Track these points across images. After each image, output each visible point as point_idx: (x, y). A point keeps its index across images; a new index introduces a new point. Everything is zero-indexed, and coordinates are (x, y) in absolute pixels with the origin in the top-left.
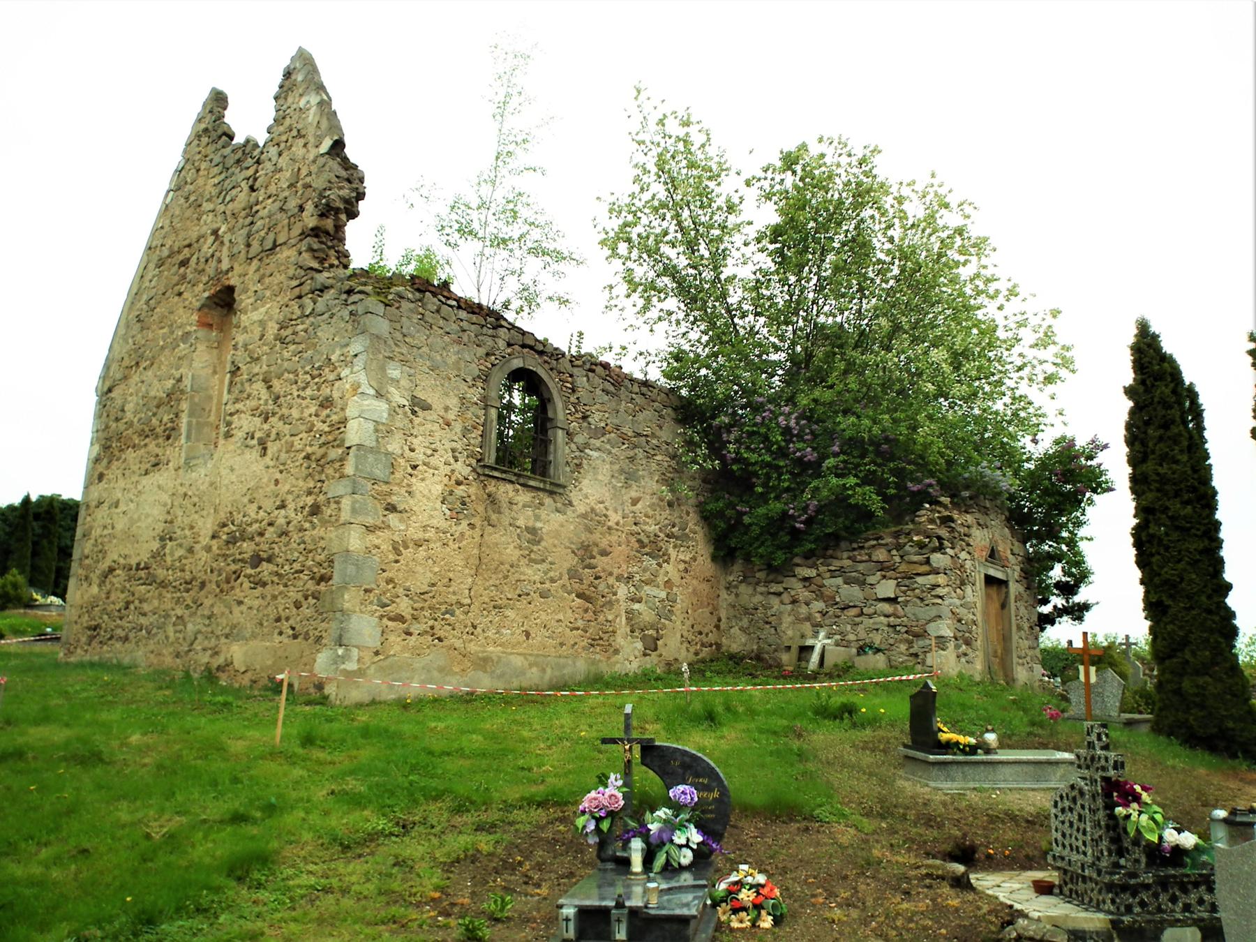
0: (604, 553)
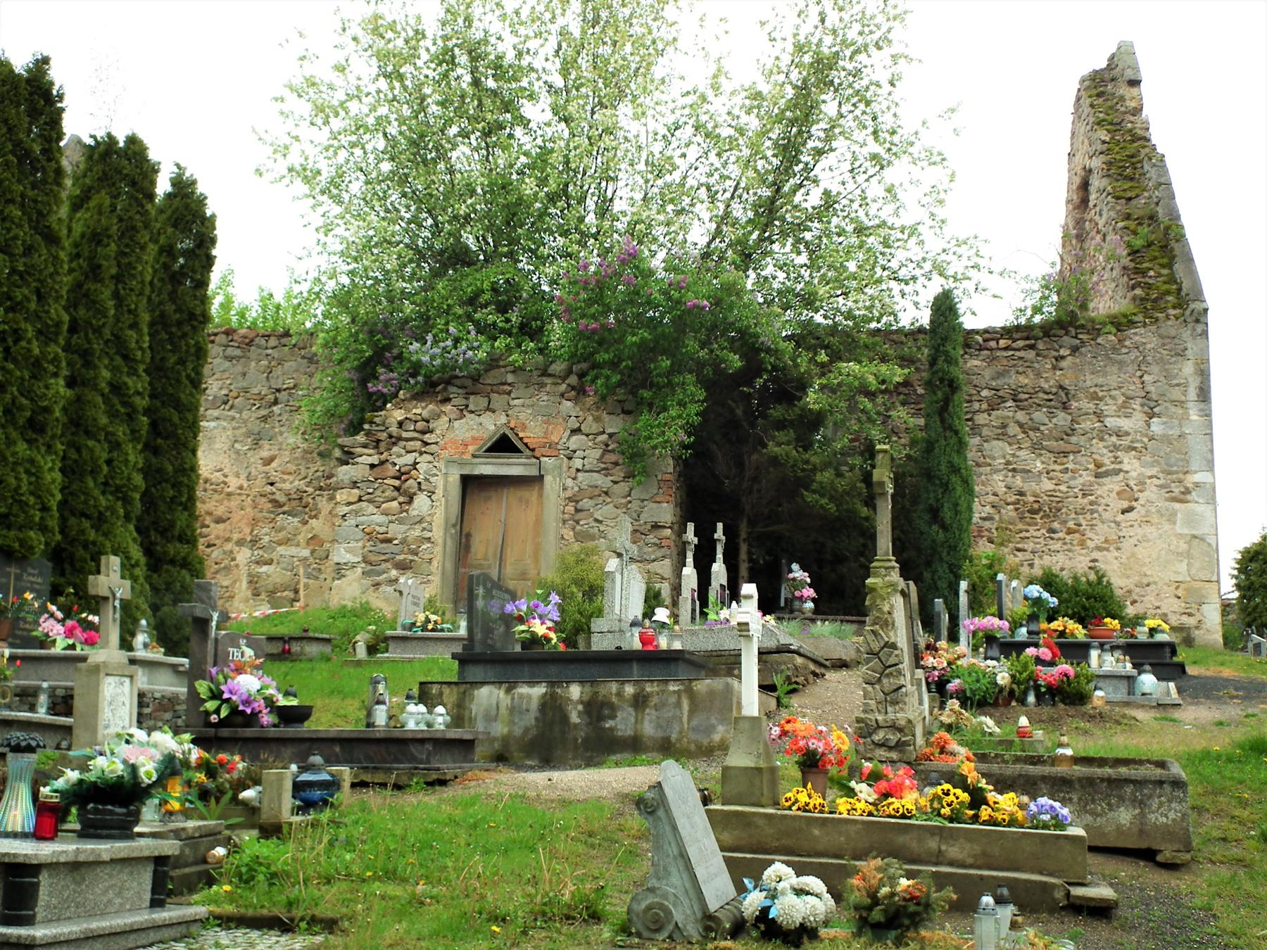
0: (219, 521)
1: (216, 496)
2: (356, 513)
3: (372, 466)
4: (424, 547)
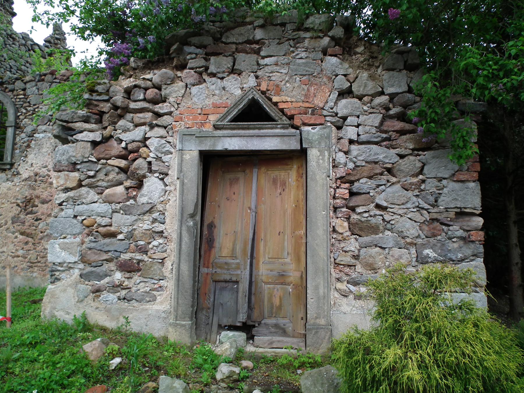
0: (44, 202)
1: (43, 185)
2: (75, 201)
3: (95, 144)
4: (155, 243)
